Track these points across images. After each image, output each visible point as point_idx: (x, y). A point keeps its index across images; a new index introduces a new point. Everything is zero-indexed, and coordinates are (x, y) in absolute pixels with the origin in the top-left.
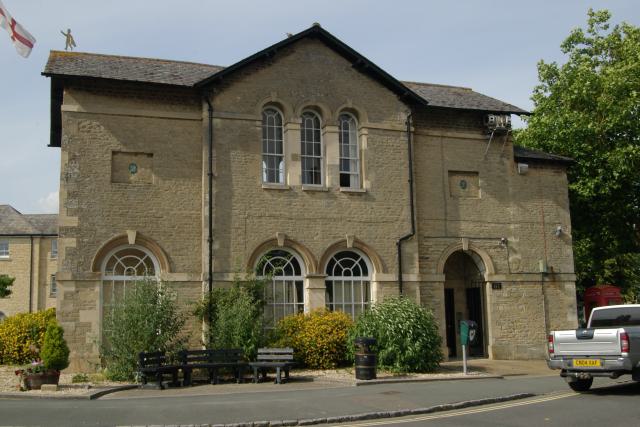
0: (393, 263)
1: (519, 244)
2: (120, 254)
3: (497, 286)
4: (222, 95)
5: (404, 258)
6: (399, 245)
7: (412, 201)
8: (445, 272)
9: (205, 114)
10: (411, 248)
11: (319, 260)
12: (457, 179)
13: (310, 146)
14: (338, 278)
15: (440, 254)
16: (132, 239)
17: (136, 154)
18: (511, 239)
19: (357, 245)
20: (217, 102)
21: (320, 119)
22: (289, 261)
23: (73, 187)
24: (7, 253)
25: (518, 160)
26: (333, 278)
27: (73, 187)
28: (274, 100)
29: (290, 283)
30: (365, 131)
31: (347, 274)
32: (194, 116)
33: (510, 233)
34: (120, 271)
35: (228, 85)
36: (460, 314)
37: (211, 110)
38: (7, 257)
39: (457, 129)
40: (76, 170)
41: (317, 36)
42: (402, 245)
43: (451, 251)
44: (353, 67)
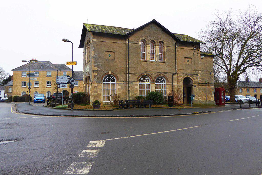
0: (170, 80)
1: (201, 76)
2: (107, 77)
3: (195, 86)
4: (131, 37)
5: (174, 79)
6: (173, 76)
7: (176, 65)
8: (183, 83)
9: (127, 42)
10: (175, 76)
11: (153, 79)
12: (187, 59)
13: (151, 50)
14: (158, 83)
15: (182, 78)
16: (110, 73)
17: (110, 52)
18: (199, 75)
19: (163, 76)
20: (130, 39)
21: (145, 43)
22: (112, 78)
23: (96, 60)
24: (38, 75)
25: (201, 55)
26: (141, 83)
27: (96, 60)
28: (144, 39)
29: (163, 85)
30: (165, 47)
31: (109, 81)
32: (124, 42)
33: (199, 73)
34: (107, 81)
35: (133, 35)
36: (185, 93)
37: (128, 41)
38: (26, 76)
39: (188, 47)
40: (96, 56)
41: (154, 22)
42: (173, 76)
43: (184, 78)
44: (163, 30)
